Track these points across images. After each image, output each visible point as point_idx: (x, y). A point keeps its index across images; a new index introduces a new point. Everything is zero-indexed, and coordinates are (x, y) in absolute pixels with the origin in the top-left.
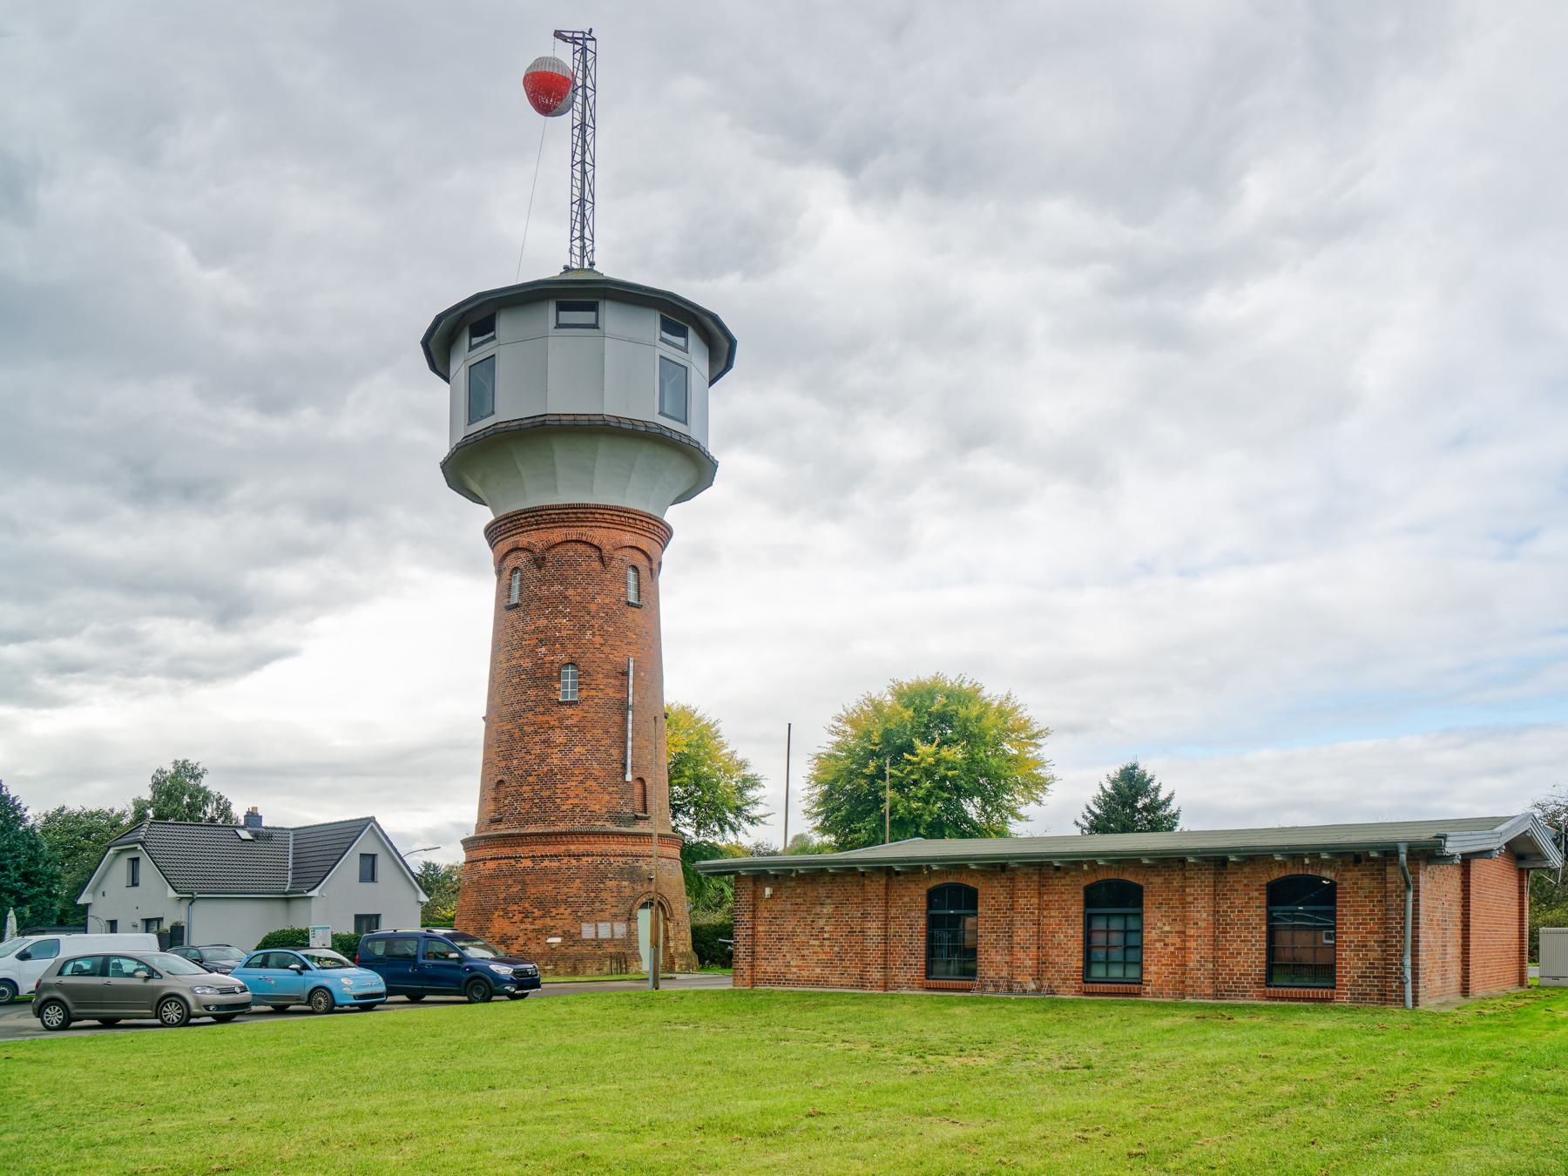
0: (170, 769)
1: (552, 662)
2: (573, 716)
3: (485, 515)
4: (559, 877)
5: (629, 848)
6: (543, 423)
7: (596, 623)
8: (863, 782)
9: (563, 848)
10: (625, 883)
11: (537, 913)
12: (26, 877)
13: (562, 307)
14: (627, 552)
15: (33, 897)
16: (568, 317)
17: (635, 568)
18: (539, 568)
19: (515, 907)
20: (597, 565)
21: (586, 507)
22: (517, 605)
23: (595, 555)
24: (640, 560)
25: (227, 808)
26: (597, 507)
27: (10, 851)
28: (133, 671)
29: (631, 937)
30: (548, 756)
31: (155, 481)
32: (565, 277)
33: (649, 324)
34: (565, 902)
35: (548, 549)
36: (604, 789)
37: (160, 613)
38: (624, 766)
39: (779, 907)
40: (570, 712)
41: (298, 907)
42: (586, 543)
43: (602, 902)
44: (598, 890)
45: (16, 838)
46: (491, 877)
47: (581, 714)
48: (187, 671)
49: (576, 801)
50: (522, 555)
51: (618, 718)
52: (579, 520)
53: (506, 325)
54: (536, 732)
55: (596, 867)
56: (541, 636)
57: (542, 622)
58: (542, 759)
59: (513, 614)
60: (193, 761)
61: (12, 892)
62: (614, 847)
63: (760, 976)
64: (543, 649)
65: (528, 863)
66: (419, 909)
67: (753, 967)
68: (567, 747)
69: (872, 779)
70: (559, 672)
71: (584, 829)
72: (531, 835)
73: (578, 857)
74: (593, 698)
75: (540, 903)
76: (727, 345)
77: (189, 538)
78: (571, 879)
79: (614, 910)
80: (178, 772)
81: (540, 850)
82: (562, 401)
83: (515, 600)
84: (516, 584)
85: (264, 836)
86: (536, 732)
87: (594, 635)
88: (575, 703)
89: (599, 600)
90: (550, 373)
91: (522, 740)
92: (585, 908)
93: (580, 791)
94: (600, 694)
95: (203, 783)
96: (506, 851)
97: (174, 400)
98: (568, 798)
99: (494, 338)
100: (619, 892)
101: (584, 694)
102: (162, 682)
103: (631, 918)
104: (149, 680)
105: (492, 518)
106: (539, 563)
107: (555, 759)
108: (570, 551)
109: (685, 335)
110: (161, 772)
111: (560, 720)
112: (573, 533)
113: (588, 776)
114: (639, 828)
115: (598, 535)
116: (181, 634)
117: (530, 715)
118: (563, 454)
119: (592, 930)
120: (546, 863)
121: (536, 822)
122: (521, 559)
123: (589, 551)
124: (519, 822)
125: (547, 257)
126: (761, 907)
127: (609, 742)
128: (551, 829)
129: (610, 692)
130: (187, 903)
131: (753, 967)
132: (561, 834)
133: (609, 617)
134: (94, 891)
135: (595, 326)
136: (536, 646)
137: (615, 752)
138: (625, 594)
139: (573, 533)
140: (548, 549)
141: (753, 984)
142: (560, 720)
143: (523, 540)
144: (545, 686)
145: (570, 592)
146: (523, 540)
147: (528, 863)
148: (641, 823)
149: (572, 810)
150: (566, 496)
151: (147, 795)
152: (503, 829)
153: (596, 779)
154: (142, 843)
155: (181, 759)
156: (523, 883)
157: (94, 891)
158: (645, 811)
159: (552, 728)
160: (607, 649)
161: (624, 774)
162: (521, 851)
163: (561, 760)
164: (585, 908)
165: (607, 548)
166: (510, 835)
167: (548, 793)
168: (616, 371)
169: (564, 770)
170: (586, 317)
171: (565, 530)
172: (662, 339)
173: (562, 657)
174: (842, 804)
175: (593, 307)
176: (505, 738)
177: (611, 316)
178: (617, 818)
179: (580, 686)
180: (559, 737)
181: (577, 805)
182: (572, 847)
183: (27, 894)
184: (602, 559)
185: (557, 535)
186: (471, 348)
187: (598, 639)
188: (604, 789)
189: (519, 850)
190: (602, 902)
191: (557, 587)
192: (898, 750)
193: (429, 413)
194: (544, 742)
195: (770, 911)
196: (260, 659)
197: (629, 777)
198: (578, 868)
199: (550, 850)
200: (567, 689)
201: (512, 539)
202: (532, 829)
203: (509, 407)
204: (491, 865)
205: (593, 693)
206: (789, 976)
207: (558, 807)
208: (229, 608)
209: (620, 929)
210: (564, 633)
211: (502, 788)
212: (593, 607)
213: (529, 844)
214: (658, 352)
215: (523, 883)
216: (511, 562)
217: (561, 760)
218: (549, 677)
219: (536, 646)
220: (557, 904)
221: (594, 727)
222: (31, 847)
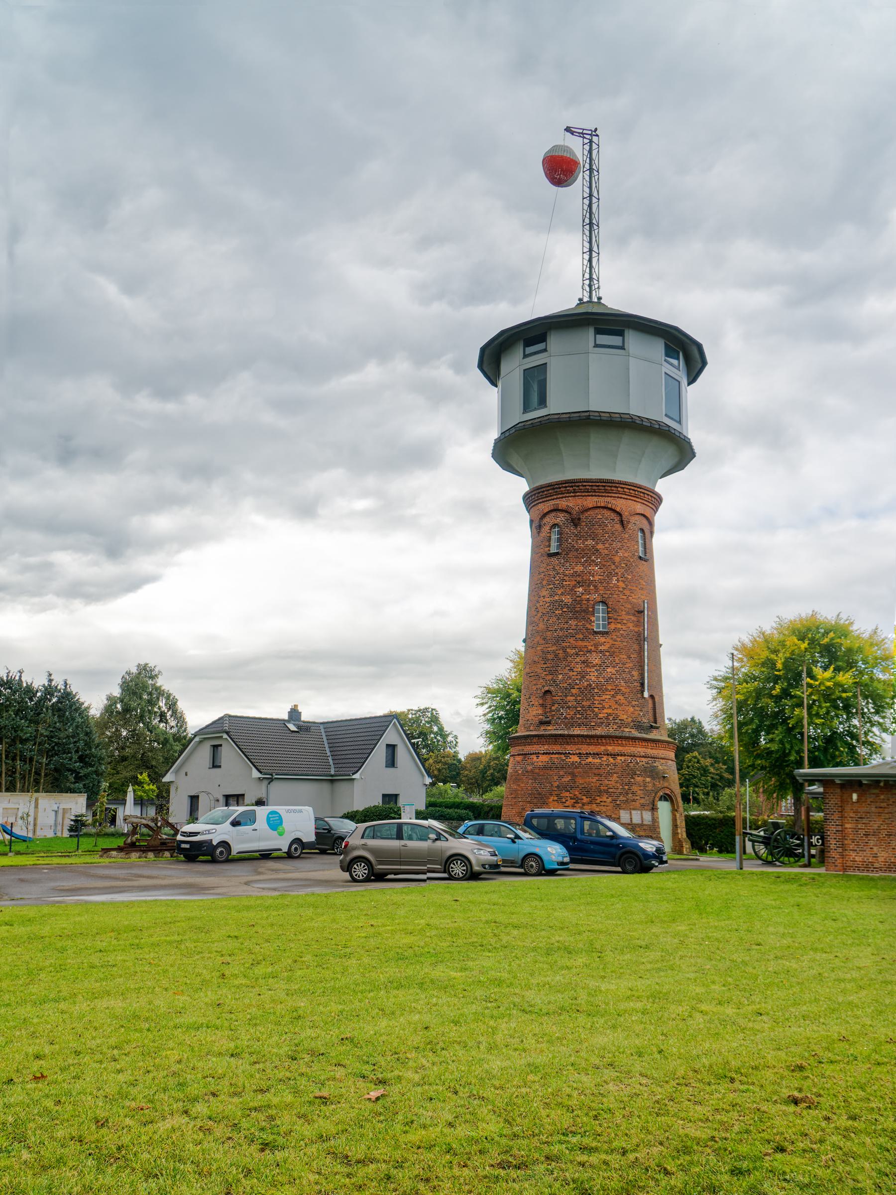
0: (134, 670)
1: (588, 600)
2: (605, 643)
3: (522, 486)
4: (601, 772)
5: (650, 752)
6: (588, 417)
7: (620, 571)
8: (769, 701)
9: (603, 748)
10: (648, 779)
11: (585, 800)
12: (81, 759)
13: (599, 332)
14: (637, 518)
15: (86, 776)
16: (603, 339)
17: (642, 530)
18: (576, 525)
19: (567, 794)
20: (618, 526)
21: (612, 482)
22: (557, 554)
23: (617, 519)
24: (644, 524)
25: (175, 704)
26: (620, 483)
27: (73, 737)
28: (36, 591)
29: (655, 820)
30: (587, 674)
31: (70, 449)
32: (582, 310)
33: (657, 347)
34: (607, 792)
35: (583, 512)
36: (630, 702)
37: (64, 548)
38: (642, 685)
39: (865, 809)
40: (602, 640)
41: (342, 787)
42: (611, 509)
43: (633, 793)
44: (629, 784)
45: (77, 727)
46: (545, 768)
47: (611, 642)
48: (79, 591)
49: (609, 711)
50: (561, 515)
51: (636, 647)
52: (606, 491)
53: (556, 342)
54: (577, 654)
55: (628, 766)
56: (578, 579)
57: (579, 568)
58: (583, 675)
59: (554, 560)
60: (151, 664)
61: (72, 771)
62: (639, 750)
63: (849, 863)
64: (581, 589)
65: (576, 759)
66: (424, 790)
67: (843, 856)
68: (601, 667)
69: (778, 699)
70: (593, 608)
71: (617, 734)
72: (578, 736)
73: (614, 756)
74: (619, 630)
75: (587, 792)
76: (700, 366)
77: (91, 492)
78: (609, 774)
79: (642, 801)
80: (140, 673)
81: (585, 749)
82: (600, 401)
83: (553, 550)
84: (554, 537)
85: (306, 728)
86: (577, 654)
87: (618, 580)
88: (607, 633)
89: (620, 554)
90: (585, 379)
91: (565, 659)
92: (622, 798)
93: (612, 703)
94: (624, 627)
95: (160, 682)
96: (557, 748)
97: (98, 390)
98: (604, 708)
99: (545, 350)
100: (645, 786)
101: (613, 626)
102: (60, 601)
103: (654, 809)
104: (50, 598)
105: (527, 489)
106: (575, 522)
107: (593, 676)
108: (600, 515)
109: (678, 359)
110: (128, 673)
111: (596, 646)
112: (602, 501)
113: (618, 691)
114: (654, 735)
115: (620, 504)
116: (71, 563)
117: (572, 640)
118: (596, 440)
119: (628, 816)
120: (590, 759)
121: (579, 725)
122: (561, 518)
123: (613, 515)
124: (566, 725)
125: (559, 296)
126: (848, 808)
127: (631, 665)
128: (593, 733)
129: (631, 625)
130: (266, 782)
131: (843, 856)
132: (602, 737)
133: (628, 567)
134: (177, 772)
135: (622, 348)
136: (575, 586)
137: (635, 673)
138: (637, 551)
139: (602, 501)
140: (583, 512)
141: (845, 870)
142: (596, 646)
143: (563, 503)
144: (584, 619)
145: (600, 546)
146: (563, 503)
147: (576, 759)
148: (655, 731)
149: (607, 718)
150: (596, 472)
151: (117, 692)
152: (551, 730)
153: (623, 694)
154: (227, 733)
155: (142, 663)
156: (573, 775)
157: (177, 772)
158: (656, 723)
159: (590, 651)
160: (627, 593)
161: (643, 692)
162: (569, 748)
163: (598, 677)
164: (622, 798)
165: (625, 514)
166: (560, 735)
167: (588, 703)
168: (625, 381)
169: (600, 686)
170: (616, 340)
171: (595, 499)
172: (665, 360)
173: (595, 596)
174: (752, 720)
175: (620, 333)
176: (550, 657)
177: (632, 339)
178: (639, 727)
179: (609, 620)
180: (595, 659)
181: (610, 715)
182: (610, 748)
183: (83, 772)
184: (622, 522)
185: (590, 502)
186: (525, 356)
187: (621, 584)
188: (630, 702)
189: (568, 747)
190: (633, 793)
191: (590, 542)
192: (793, 674)
193: (486, 408)
194: (583, 662)
195: (856, 812)
196: (133, 584)
197: (646, 695)
198: (615, 765)
199: (592, 749)
200: (599, 621)
201: (553, 502)
202: (577, 731)
203: (559, 402)
204: (545, 758)
205: (619, 626)
206: (876, 865)
207: (596, 715)
208: (115, 545)
209: (647, 816)
210: (597, 578)
211: (548, 697)
212: (617, 559)
213: (575, 744)
214: (664, 370)
215: (573, 775)
216: (550, 520)
217: (598, 677)
218: (586, 611)
219: (575, 586)
220: (600, 793)
221: (620, 653)
222: (87, 734)
